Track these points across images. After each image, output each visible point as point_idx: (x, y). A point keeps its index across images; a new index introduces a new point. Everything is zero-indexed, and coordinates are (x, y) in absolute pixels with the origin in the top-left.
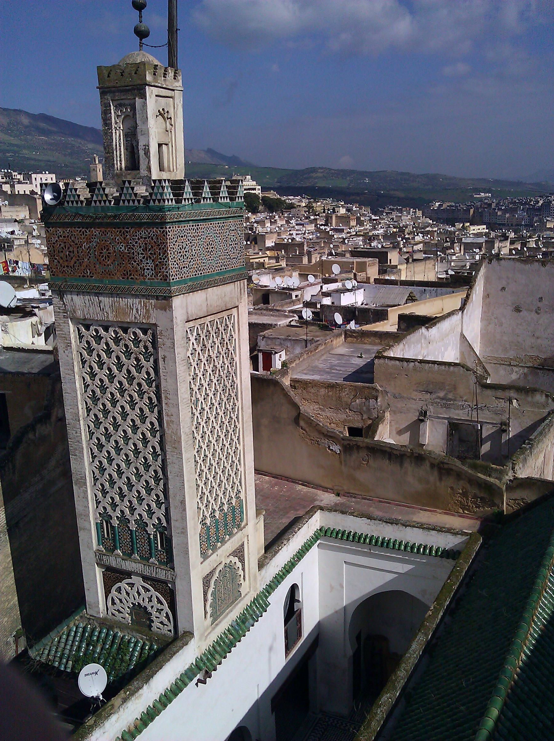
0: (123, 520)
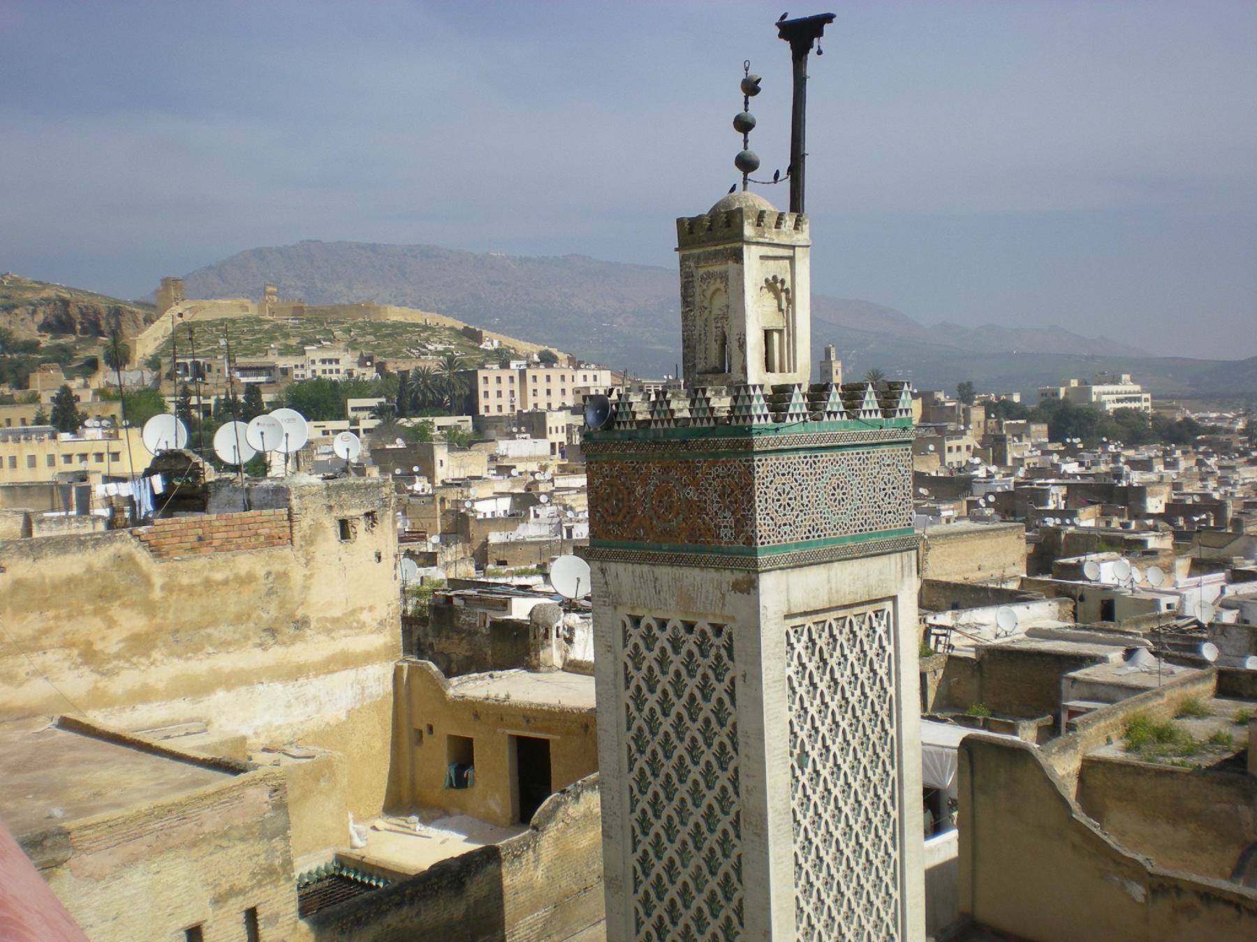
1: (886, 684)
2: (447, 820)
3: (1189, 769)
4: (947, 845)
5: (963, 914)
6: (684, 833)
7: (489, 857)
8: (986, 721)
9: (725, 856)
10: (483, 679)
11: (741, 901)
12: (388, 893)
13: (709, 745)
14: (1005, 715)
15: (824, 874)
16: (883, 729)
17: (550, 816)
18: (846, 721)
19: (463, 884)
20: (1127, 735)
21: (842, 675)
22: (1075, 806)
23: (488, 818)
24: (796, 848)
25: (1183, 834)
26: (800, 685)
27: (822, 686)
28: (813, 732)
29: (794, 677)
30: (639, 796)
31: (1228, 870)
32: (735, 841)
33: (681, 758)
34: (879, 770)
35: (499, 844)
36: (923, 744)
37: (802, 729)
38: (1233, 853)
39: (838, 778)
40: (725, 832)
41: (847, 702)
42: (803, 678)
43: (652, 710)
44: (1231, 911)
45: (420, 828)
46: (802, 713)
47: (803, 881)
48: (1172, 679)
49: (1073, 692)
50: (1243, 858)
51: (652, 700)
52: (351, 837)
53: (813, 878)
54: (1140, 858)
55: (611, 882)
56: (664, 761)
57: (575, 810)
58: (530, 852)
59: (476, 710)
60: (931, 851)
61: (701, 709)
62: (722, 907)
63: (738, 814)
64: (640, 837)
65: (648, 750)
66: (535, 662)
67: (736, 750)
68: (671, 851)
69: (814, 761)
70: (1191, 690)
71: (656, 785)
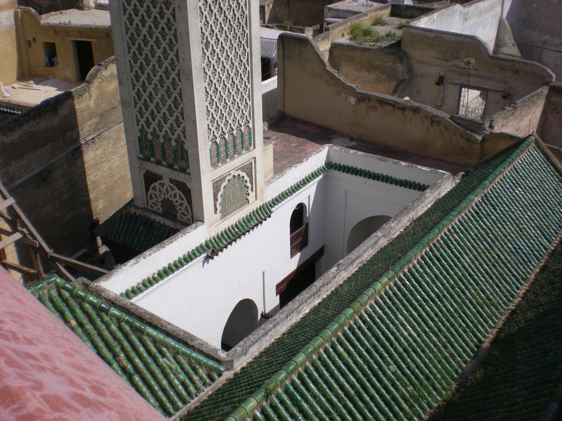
0: (154, 134)
1: (244, 9)
2: (47, 81)
3: (376, 48)
4: (272, 83)
5: (280, 112)
6: (155, 80)
7: (67, 97)
8: (291, 28)
9: (175, 89)
10: (57, 14)
11: (182, 108)
12: (22, 116)
13: (165, 40)
14: (299, 25)
15: (218, 95)
16: (243, 30)
17: (94, 76)
18: (227, 26)
19: (57, 109)
20: (351, 33)
21: (224, 6)
22: (327, 64)
23: (65, 80)
24: (206, 84)
25: (373, 76)
26: (205, 10)
27: (215, 11)
28: (211, 32)
29: (202, 7)
30: (134, 65)
31: (391, 91)
32: (179, 83)
33: (152, 46)
34: (242, 49)
35: (72, 90)
36: (261, 38)
37: (206, 31)
38: (393, 84)
39: (223, 53)
40: (174, 79)
41: (227, 18)
42: (206, 7)
43: (137, 25)
44: (391, 108)
45: (34, 86)
46: (206, 23)
47: (209, 99)
48: (372, 8)
49: (329, 14)
50: (397, 86)
51: (137, 20)
52: (3, 92)
53: (213, 97)
54: (354, 86)
55: (124, 104)
56: (144, 48)
57: (105, 73)
58: (87, 93)
59: (56, 29)
60: (266, 85)
61: (160, 23)
62: (174, 112)
63: (179, 70)
64: (136, 83)
65: (137, 44)
66: (81, 5)
67: (177, 41)
68: (150, 88)
69: (212, 45)
70: (380, 13)
71: (141, 59)
